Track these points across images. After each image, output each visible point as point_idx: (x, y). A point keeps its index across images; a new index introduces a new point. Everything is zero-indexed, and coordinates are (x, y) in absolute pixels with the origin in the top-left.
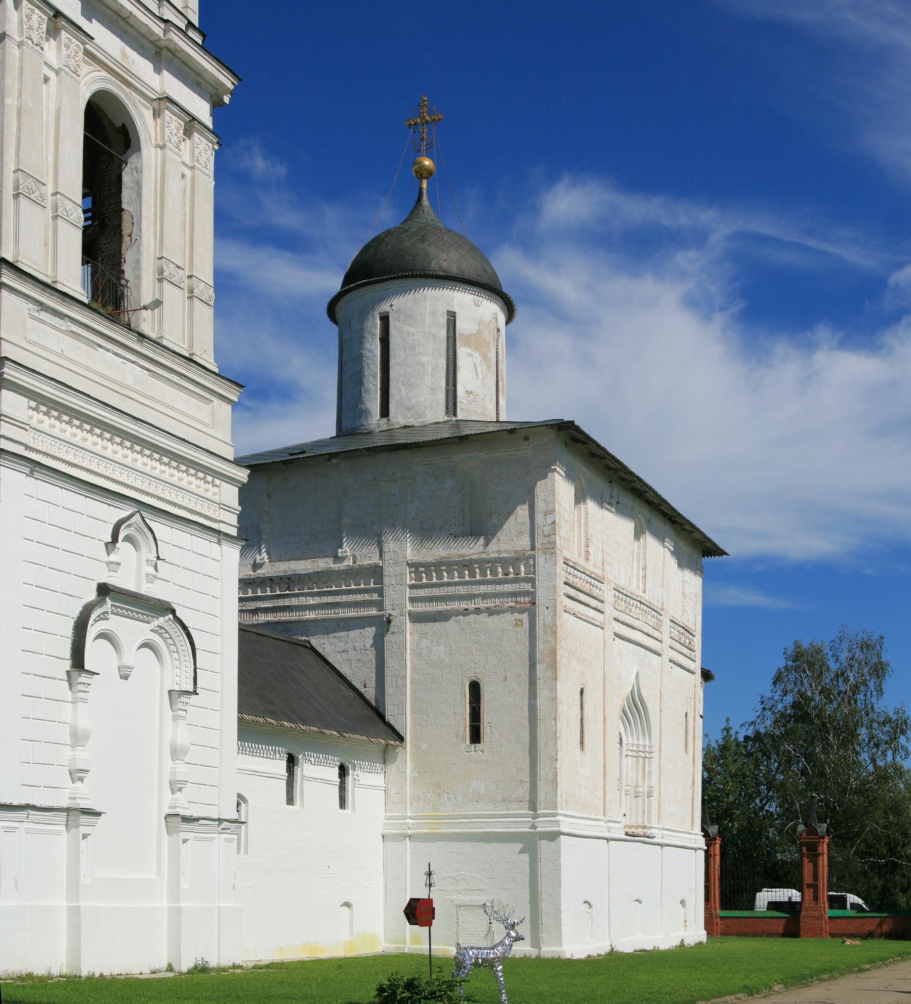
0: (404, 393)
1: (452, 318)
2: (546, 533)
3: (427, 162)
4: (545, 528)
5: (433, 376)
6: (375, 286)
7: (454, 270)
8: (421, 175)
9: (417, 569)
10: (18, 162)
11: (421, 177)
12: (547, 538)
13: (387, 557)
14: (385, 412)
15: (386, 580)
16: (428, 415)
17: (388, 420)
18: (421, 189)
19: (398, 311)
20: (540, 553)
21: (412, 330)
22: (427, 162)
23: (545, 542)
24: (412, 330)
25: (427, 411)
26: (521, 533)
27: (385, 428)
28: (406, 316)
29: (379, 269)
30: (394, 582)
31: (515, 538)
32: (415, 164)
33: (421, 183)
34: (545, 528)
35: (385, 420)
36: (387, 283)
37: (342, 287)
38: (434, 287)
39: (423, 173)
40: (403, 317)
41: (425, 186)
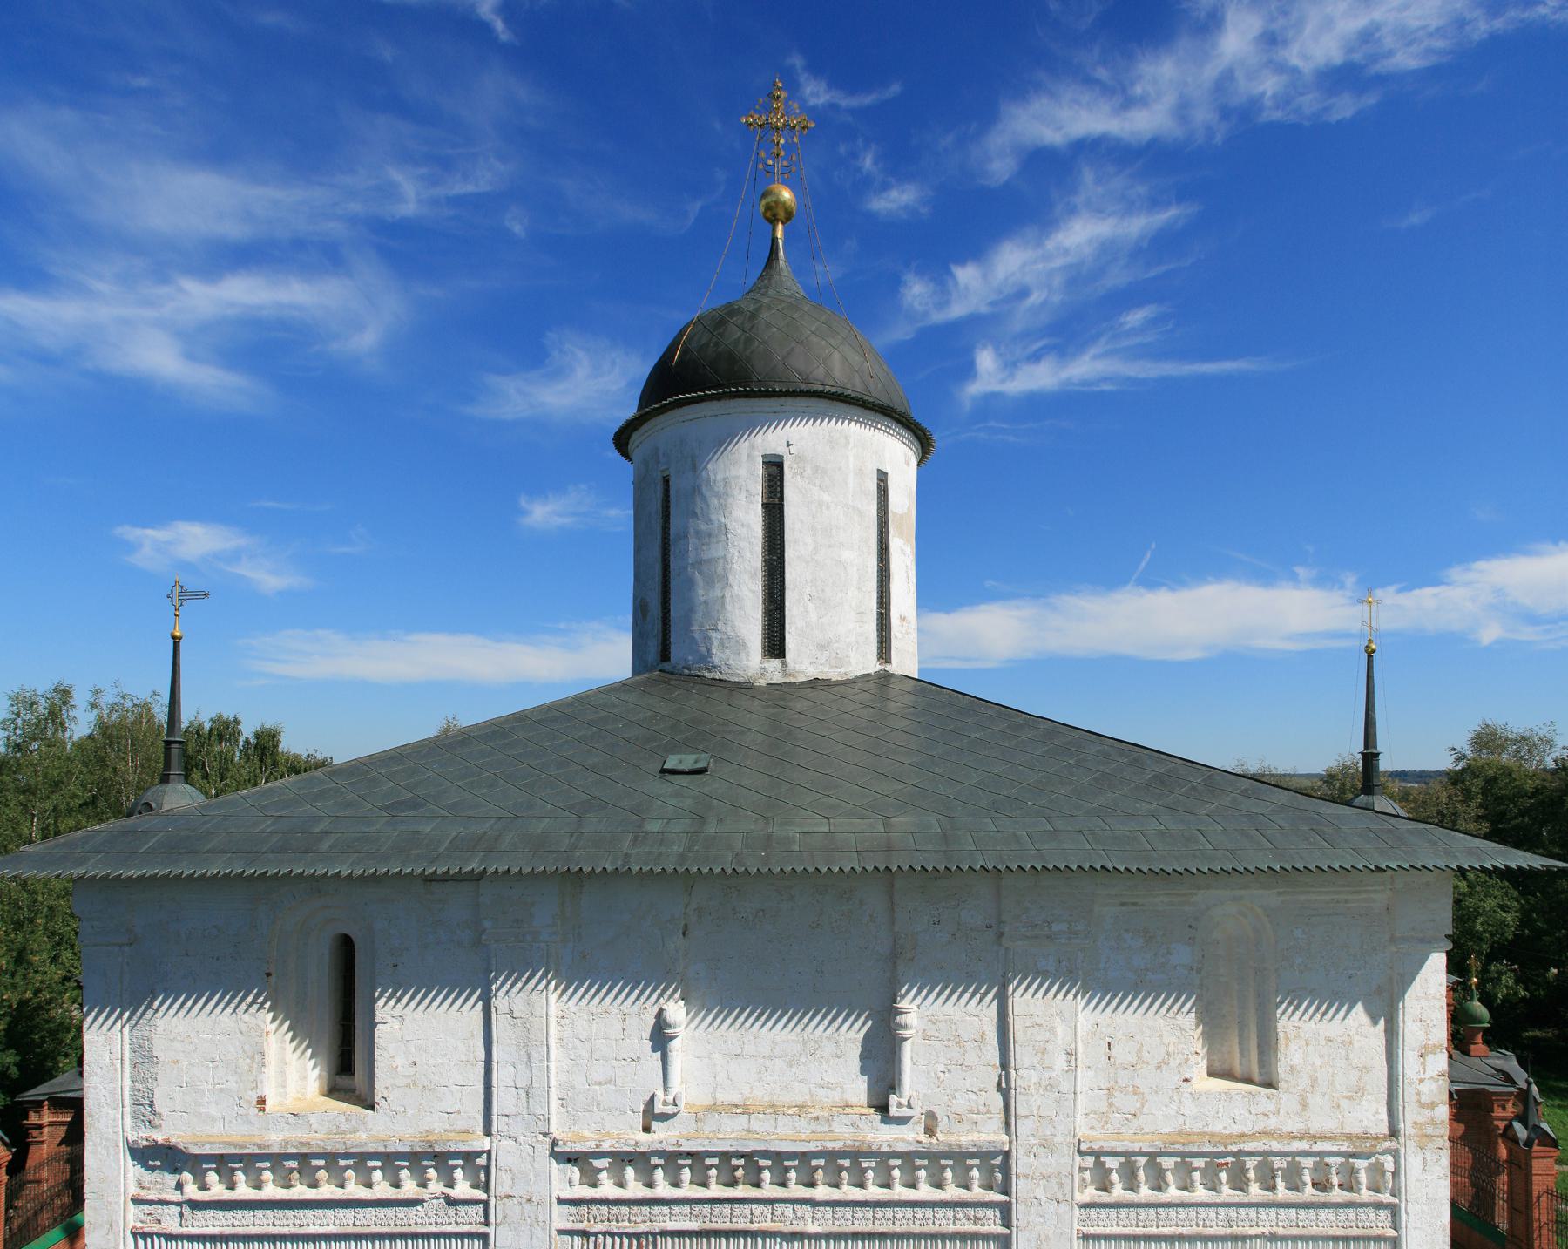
0: (813, 616)
1: (774, 470)
2: (1424, 1099)
3: (786, 195)
4: (1422, 1087)
5: (859, 589)
6: (686, 409)
7: (856, 387)
8: (775, 215)
9: (1099, 1164)
10: (146, 1110)
11: (773, 221)
12: (1427, 1112)
13: (1023, 1128)
14: (775, 645)
15: (1020, 1187)
16: (853, 661)
17: (784, 664)
18: (774, 240)
19: (799, 458)
20: (1412, 1145)
21: (826, 497)
22: (786, 195)
23: (1420, 1119)
24: (826, 497)
25: (852, 654)
26: (1358, 1093)
27: (777, 678)
28: (816, 468)
29: (707, 377)
30: (1040, 1193)
31: (1344, 1103)
32: (764, 196)
33: (774, 230)
34: (1422, 1087)
35: (776, 663)
36: (782, 400)
37: (640, 407)
38: (816, 416)
39: (774, 214)
40: (809, 471)
41: (779, 234)
